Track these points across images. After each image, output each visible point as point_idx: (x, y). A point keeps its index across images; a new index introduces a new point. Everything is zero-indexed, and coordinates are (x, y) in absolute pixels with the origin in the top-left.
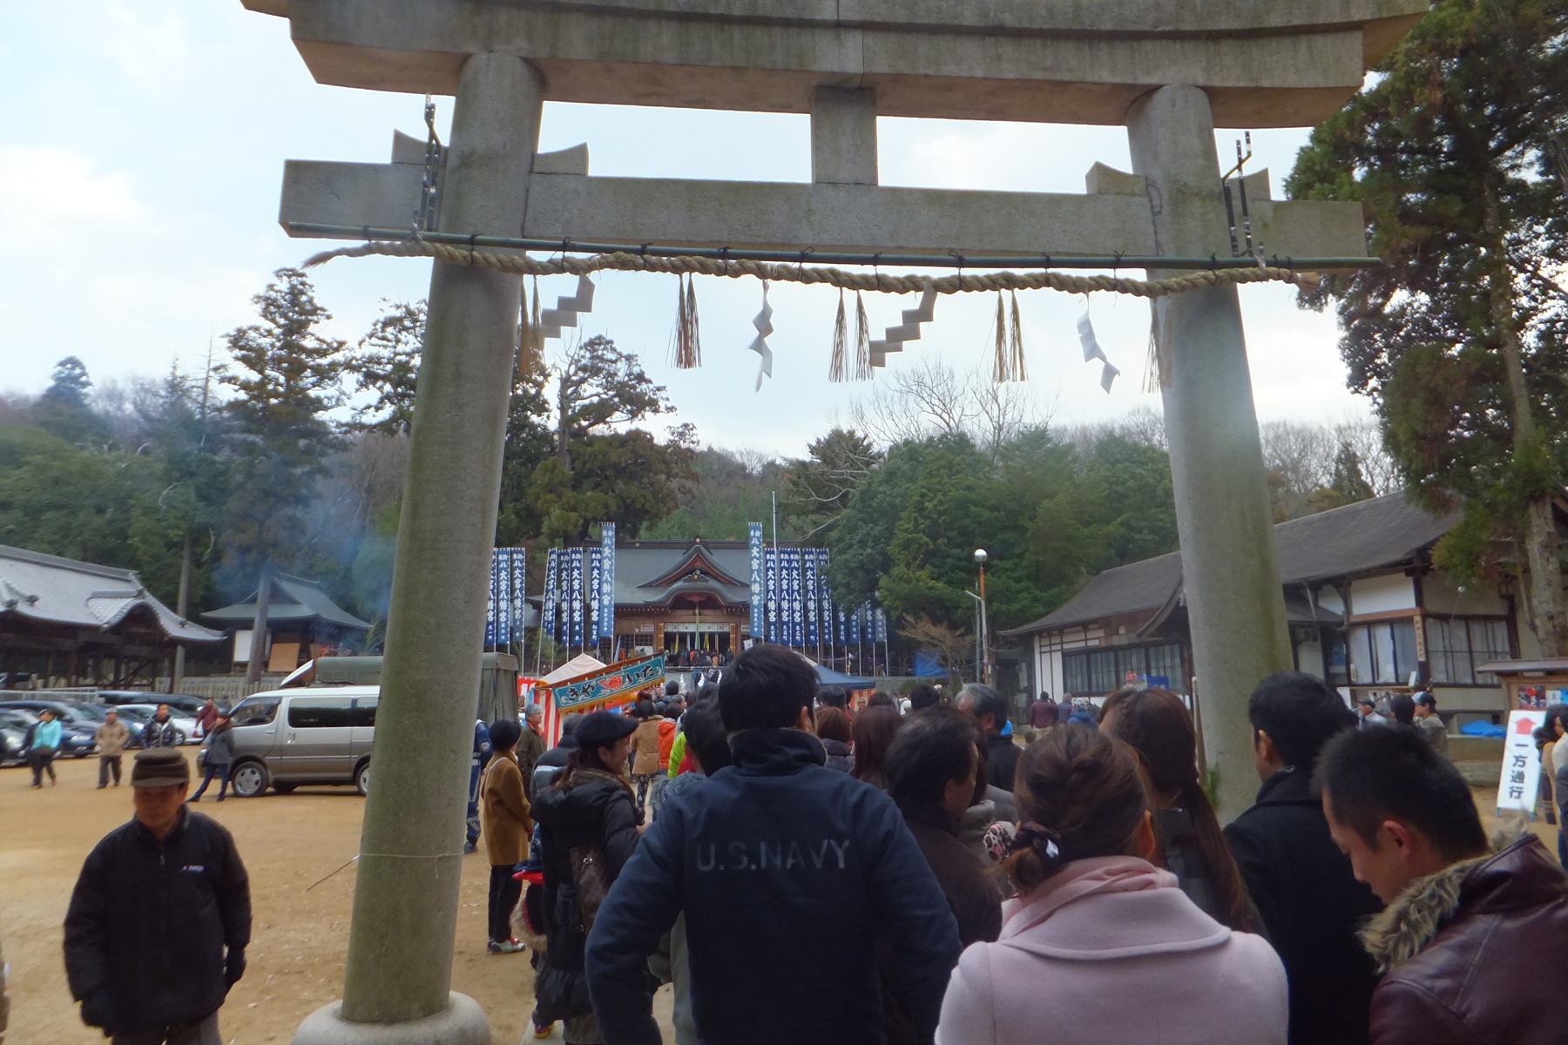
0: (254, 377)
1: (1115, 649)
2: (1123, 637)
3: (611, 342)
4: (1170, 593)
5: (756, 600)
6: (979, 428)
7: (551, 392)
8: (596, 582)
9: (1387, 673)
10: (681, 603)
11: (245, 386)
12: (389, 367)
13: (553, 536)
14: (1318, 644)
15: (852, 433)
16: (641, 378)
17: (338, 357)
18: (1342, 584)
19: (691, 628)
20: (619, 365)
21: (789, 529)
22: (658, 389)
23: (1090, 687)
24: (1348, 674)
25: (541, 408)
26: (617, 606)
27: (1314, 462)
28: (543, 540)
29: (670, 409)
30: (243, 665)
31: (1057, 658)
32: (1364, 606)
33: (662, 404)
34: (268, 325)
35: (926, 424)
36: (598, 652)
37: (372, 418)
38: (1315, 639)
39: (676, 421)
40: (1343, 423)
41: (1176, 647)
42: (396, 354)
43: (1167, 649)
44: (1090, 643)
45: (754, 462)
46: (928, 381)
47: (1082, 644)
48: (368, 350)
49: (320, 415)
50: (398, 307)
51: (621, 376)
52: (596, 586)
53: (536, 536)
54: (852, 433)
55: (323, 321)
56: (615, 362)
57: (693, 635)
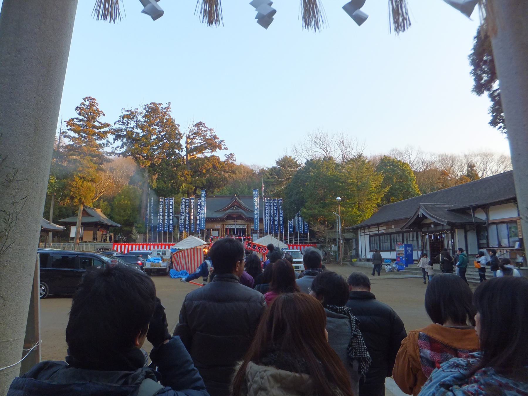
0: (76, 136)
1: (390, 234)
2: (393, 229)
3: (204, 124)
4: (415, 211)
5: (256, 216)
6: (337, 156)
7: (183, 142)
8: (199, 210)
9: (505, 242)
10: (230, 217)
11: (73, 139)
12: (125, 133)
13: (184, 193)
14: (475, 232)
15: (290, 157)
16: (215, 137)
17: (107, 129)
18: (485, 208)
19: (233, 227)
20: (207, 132)
21: (268, 190)
22: (222, 141)
23: (380, 247)
24: (488, 243)
25: (179, 147)
26: (206, 218)
27: (456, 168)
28: (180, 194)
29: (225, 149)
30: (73, 238)
31: (367, 238)
32: (495, 216)
33: (223, 147)
34: (81, 117)
35: (319, 154)
36: (200, 235)
37: (118, 151)
38: (474, 230)
39: (228, 153)
40: (467, 153)
41: (415, 233)
42: (127, 128)
43: (411, 234)
44: (380, 232)
45: (256, 169)
46: (319, 136)
47: (377, 232)
48: (117, 126)
49: (101, 150)
50: (128, 111)
51: (208, 137)
52: (199, 211)
53: (178, 193)
54: (290, 157)
55: (101, 116)
56: (206, 131)
57: (234, 229)
